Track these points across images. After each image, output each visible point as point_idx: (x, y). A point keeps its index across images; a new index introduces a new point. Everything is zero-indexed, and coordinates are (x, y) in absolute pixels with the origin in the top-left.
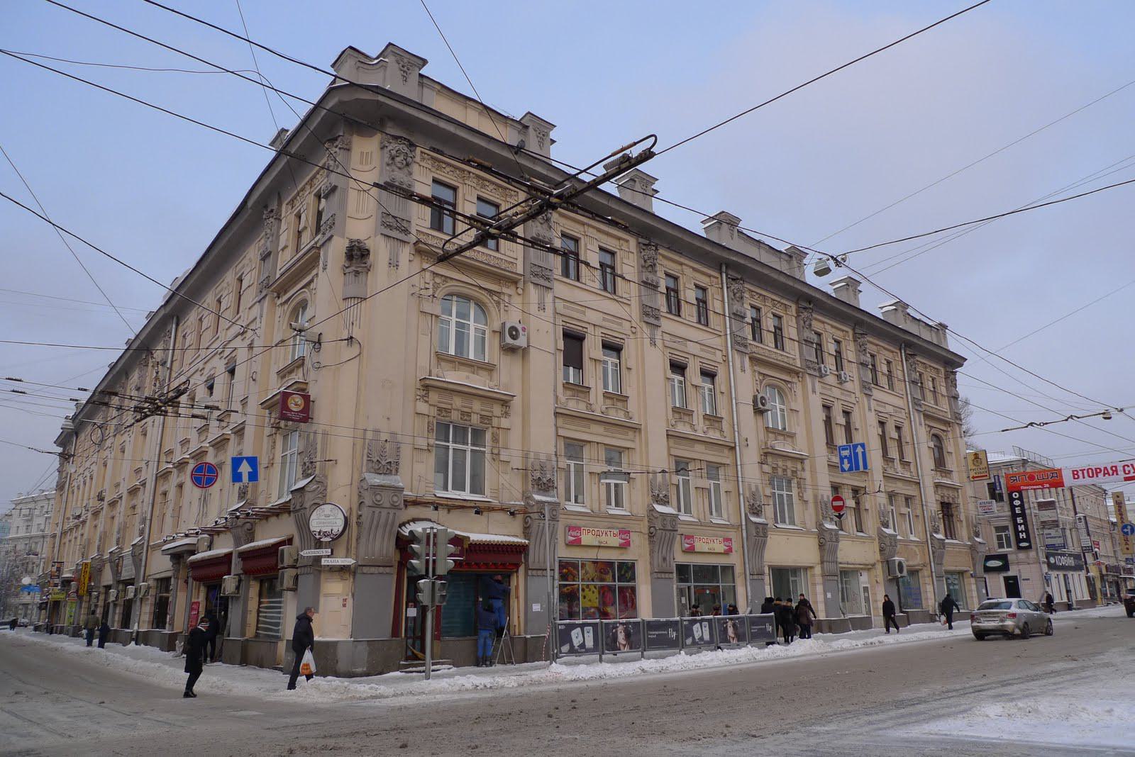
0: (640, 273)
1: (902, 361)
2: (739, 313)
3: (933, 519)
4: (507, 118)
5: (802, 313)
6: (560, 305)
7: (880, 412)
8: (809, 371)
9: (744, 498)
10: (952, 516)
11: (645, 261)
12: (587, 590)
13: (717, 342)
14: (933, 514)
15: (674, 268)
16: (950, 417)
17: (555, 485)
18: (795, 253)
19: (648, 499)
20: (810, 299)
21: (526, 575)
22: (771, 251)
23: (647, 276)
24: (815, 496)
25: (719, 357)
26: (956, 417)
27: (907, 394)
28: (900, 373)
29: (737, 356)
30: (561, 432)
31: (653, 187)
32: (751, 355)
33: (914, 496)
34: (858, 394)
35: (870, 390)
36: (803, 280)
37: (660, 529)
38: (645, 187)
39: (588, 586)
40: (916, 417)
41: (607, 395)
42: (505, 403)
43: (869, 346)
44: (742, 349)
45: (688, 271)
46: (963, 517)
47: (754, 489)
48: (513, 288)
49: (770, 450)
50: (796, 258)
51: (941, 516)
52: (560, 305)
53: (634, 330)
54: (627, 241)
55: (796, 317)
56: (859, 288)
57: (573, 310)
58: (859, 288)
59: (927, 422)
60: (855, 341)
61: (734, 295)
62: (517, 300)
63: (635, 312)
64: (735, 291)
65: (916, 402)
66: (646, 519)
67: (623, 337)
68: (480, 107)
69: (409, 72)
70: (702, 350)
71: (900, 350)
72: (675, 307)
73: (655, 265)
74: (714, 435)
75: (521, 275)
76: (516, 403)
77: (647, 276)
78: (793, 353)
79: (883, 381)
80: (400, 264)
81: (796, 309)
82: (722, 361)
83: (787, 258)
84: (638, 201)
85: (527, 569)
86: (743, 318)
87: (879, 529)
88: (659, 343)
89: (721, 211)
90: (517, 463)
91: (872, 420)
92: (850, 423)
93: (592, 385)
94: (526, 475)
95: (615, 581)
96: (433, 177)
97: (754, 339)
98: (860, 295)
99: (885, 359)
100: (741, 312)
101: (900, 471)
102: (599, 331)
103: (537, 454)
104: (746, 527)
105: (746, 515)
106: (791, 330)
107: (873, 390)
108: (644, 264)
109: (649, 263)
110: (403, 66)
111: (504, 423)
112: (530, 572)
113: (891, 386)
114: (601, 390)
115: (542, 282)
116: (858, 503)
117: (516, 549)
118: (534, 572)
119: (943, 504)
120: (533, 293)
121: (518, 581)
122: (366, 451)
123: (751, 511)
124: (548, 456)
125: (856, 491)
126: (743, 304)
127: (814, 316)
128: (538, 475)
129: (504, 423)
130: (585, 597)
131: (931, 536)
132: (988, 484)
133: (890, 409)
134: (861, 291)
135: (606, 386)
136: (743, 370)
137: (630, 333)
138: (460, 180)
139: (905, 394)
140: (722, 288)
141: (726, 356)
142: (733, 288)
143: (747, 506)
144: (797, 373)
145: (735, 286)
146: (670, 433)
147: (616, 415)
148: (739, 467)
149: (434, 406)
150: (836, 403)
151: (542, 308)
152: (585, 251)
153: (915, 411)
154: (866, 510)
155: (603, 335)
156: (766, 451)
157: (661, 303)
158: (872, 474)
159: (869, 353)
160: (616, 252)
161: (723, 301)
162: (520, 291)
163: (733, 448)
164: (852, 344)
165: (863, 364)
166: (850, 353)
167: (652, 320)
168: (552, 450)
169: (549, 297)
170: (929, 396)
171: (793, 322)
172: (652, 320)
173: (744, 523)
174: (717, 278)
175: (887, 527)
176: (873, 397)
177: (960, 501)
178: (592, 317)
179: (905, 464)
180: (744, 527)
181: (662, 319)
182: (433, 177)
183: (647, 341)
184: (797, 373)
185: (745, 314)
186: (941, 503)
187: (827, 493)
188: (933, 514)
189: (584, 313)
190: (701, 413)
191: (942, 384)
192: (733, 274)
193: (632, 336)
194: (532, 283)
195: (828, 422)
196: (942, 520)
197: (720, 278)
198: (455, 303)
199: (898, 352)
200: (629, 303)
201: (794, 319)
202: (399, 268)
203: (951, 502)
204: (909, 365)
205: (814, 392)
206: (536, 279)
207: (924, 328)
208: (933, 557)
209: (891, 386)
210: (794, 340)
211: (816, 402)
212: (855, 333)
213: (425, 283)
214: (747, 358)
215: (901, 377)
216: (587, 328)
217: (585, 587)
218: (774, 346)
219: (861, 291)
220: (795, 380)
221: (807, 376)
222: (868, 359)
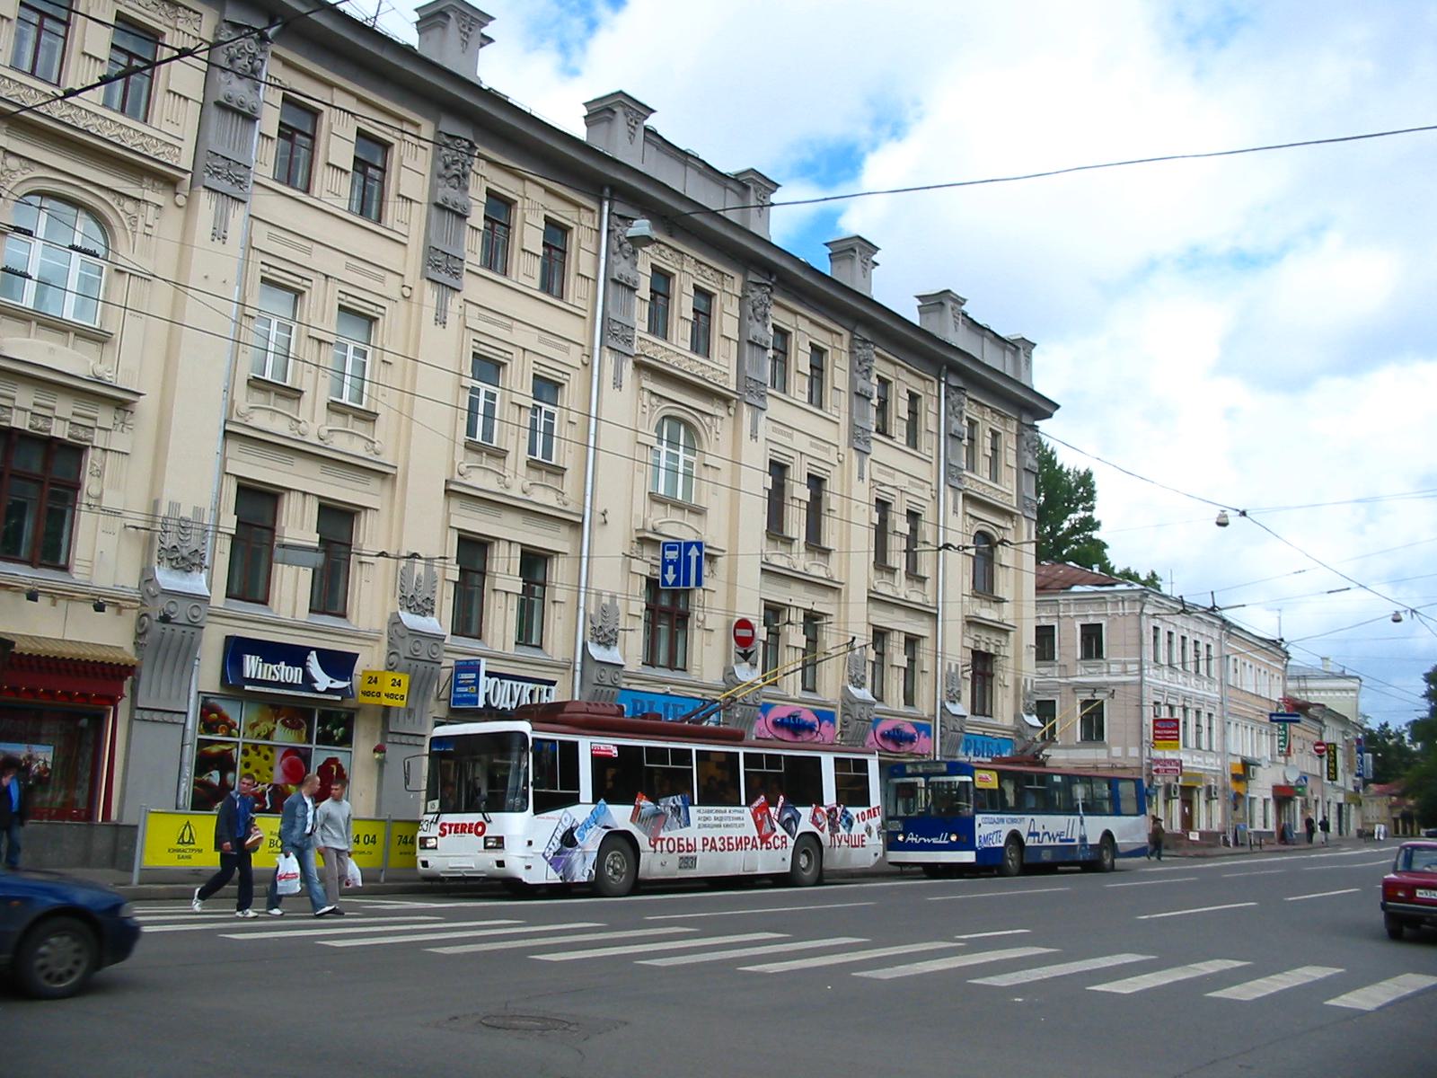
0: (433, 189)
1: (939, 397)
2: (757, 342)
3: (950, 678)
4: (685, 153)
5: (859, 348)
6: (261, 236)
7: (883, 485)
8: (749, 399)
9: (585, 614)
10: (991, 676)
11: (447, 167)
12: (252, 753)
13: (573, 328)
14: (953, 670)
15: (506, 185)
16: (1015, 505)
17: (207, 562)
18: (755, 182)
19: (393, 605)
20: (767, 268)
21: (131, 719)
22: (997, 340)
23: (449, 193)
24: (1017, 682)
25: (574, 356)
26: (1025, 506)
27: (939, 457)
28: (931, 419)
29: (609, 359)
30: (871, 621)
31: (485, 31)
32: (639, 358)
33: (923, 637)
34: (843, 447)
35: (867, 443)
36: (1027, 384)
37: (406, 658)
38: (633, 124)
39: (255, 747)
40: (948, 496)
41: (532, 465)
42: (121, 404)
43: (877, 363)
44: (621, 347)
45: (804, 325)
46: (1009, 680)
47: (606, 600)
48: (170, 193)
49: (647, 535)
50: (756, 191)
51: (968, 675)
52: (261, 236)
53: (407, 292)
54: (932, 381)
55: (740, 299)
56: (875, 258)
57: (494, 323)
58: (875, 258)
59: (969, 510)
60: (852, 353)
61: (620, 246)
62: (174, 218)
63: (410, 261)
64: (756, 303)
65: (952, 473)
66: (385, 639)
67: (829, 468)
68: (659, 142)
69: (471, 33)
70: (541, 340)
71: (940, 381)
72: (496, 255)
73: (465, 175)
74: (543, 498)
75: (186, 172)
76: (146, 407)
77: (449, 193)
78: (722, 366)
79: (899, 429)
80: (228, 235)
81: (743, 285)
82: (579, 365)
83: (738, 189)
84: (452, 61)
85: (134, 707)
86: (869, 399)
87: (845, 689)
88: (452, 319)
89: (945, 288)
90: (137, 513)
91: (863, 494)
92: (886, 521)
93: (510, 447)
94: (151, 540)
95: (310, 742)
96: (358, 128)
97: (774, 386)
98: (875, 271)
99: (991, 429)
100: (456, 205)
101: (800, 560)
102: (530, 358)
103: (174, 506)
104: (582, 667)
105: (585, 645)
106: (726, 321)
107: (873, 443)
108: (444, 172)
109: (454, 170)
110: (464, 26)
111: (118, 441)
112: (138, 714)
113: (913, 440)
114: (524, 455)
115: (224, 186)
116: (911, 661)
117: (93, 668)
118: (146, 715)
119: (976, 654)
120: (206, 205)
121: (120, 723)
122: (399, 583)
123: (595, 639)
124: (198, 511)
125: (912, 641)
126: (636, 264)
127: (776, 297)
128: (171, 541)
129: (118, 441)
130: (247, 765)
131: (943, 707)
132: (1082, 626)
133: (901, 481)
134: (876, 264)
135: (532, 451)
136: (618, 384)
137: (836, 463)
138: (678, 267)
139: (935, 456)
140: (599, 231)
141: (938, 491)
142: (752, 298)
143: (944, 692)
144: (1009, 515)
145: (955, 397)
146: (452, 487)
147: (349, 445)
148: (585, 560)
149: (65, 420)
150: (898, 499)
151: (219, 235)
152: (833, 369)
153: (949, 488)
154: (923, 672)
155: (266, 268)
156: (641, 535)
157: (472, 248)
158: (847, 592)
159: (967, 418)
160: (715, 294)
161: (597, 255)
162: (181, 200)
163: (577, 526)
164: (845, 357)
165: (956, 437)
166: (839, 372)
167: (443, 277)
168: (207, 502)
169: (238, 215)
170: (983, 464)
171: (733, 308)
172: (443, 277)
173: (579, 659)
174: (592, 211)
175: (860, 685)
176: (871, 456)
177: (1008, 651)
178: (522, 336)
179: (913, 575)
180: (578, 667)
181: (768, 399)
182: (358, 128)
183: (429, 314)
184: (1009, 515)
185: (635, 283)
186: (973, 652)
187: (864, 636)
188: (953, 670)
189: (309, 252)
190: (324, 396)
191: (1009, 445)
192: (955, 382)
193: (402, 303)
194: (205, 187)
195: (881, 531)
196: (969, 683)
197: (597, 211)
198: (44, 216)
199: (936, 381)
200: (837, 420)
201: (736, 301)
202: (447, 325)
203: (992, 651)
204: (615, 244)
205: (754, 436)
206: (437, 273)
207: (991, 341)
208: (941, 744)
209: (913, 440)
210: (729, 339)
211: (756, 457)
212: (852, 340)
213: (147, 225)
214: (630, 361)
215: (933, 428)
216: (384, 308)
217: (249, 748)
218: (806, 401)
219: (490, 40)
220: (720, 412)
221: (745, 405)
222: (874, 387)
